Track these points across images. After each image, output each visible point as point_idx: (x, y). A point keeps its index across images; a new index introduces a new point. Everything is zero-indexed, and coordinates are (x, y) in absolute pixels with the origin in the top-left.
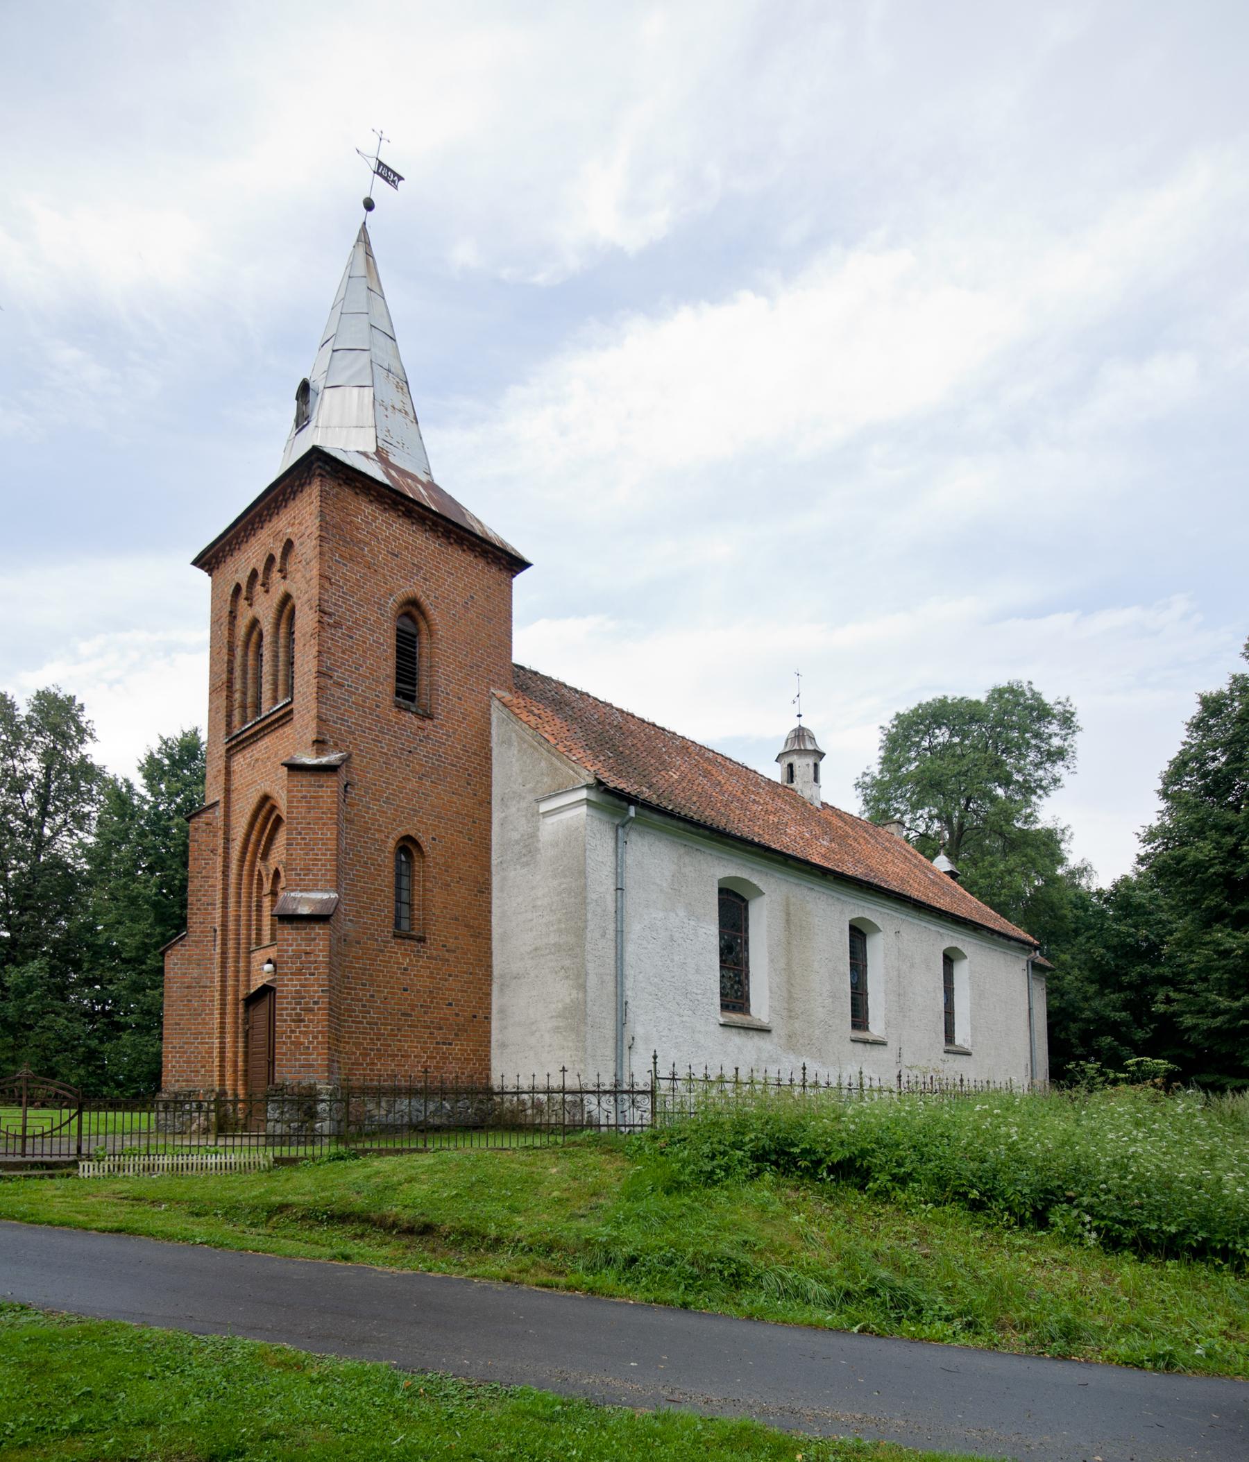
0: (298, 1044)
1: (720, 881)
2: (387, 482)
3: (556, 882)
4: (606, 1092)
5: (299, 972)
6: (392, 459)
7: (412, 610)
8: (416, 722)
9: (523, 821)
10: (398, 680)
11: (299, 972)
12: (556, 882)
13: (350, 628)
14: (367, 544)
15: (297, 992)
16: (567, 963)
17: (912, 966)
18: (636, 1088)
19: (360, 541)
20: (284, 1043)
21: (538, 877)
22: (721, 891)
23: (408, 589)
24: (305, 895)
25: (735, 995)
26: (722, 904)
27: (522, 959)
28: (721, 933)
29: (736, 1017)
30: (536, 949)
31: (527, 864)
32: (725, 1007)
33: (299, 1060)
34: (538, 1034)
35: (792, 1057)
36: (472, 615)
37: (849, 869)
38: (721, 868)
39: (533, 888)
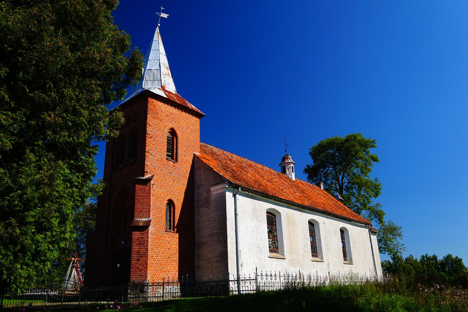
0: (138, 268)
1: (267, 210)
2: (166, 97)
3: (216, 213)
4: (247, 280)
5: (139, 244)
6: (167, 89)
7: (173, 132)
8: (172, 164)
9: (205, 193)
10: (167, 152)
11: (139, 244)
12: (216, 213)
13: (155, 138)
14: (160, 114)
15: (138, 251)
16: (221, 239)
17: (330, 234)
18: (251, 279)
19: (158, 113)
20: (133, 268)
21: (210, 211)
22: (267, 213)
23: (171, 126)
24: (140, 219)
25: (315, 250)
26: (268, 218)
27: (206, 238)
28: (268, 227)
29: (274, 254)
30: (210, 234)
31: (207, 207)
32: (270, 251)
33: (137, 273)
34: (211, 263)
35: (293, 268)
36: (188, 131)
37: (307, 203)
38: (265, 206)
39: (209, 214)
